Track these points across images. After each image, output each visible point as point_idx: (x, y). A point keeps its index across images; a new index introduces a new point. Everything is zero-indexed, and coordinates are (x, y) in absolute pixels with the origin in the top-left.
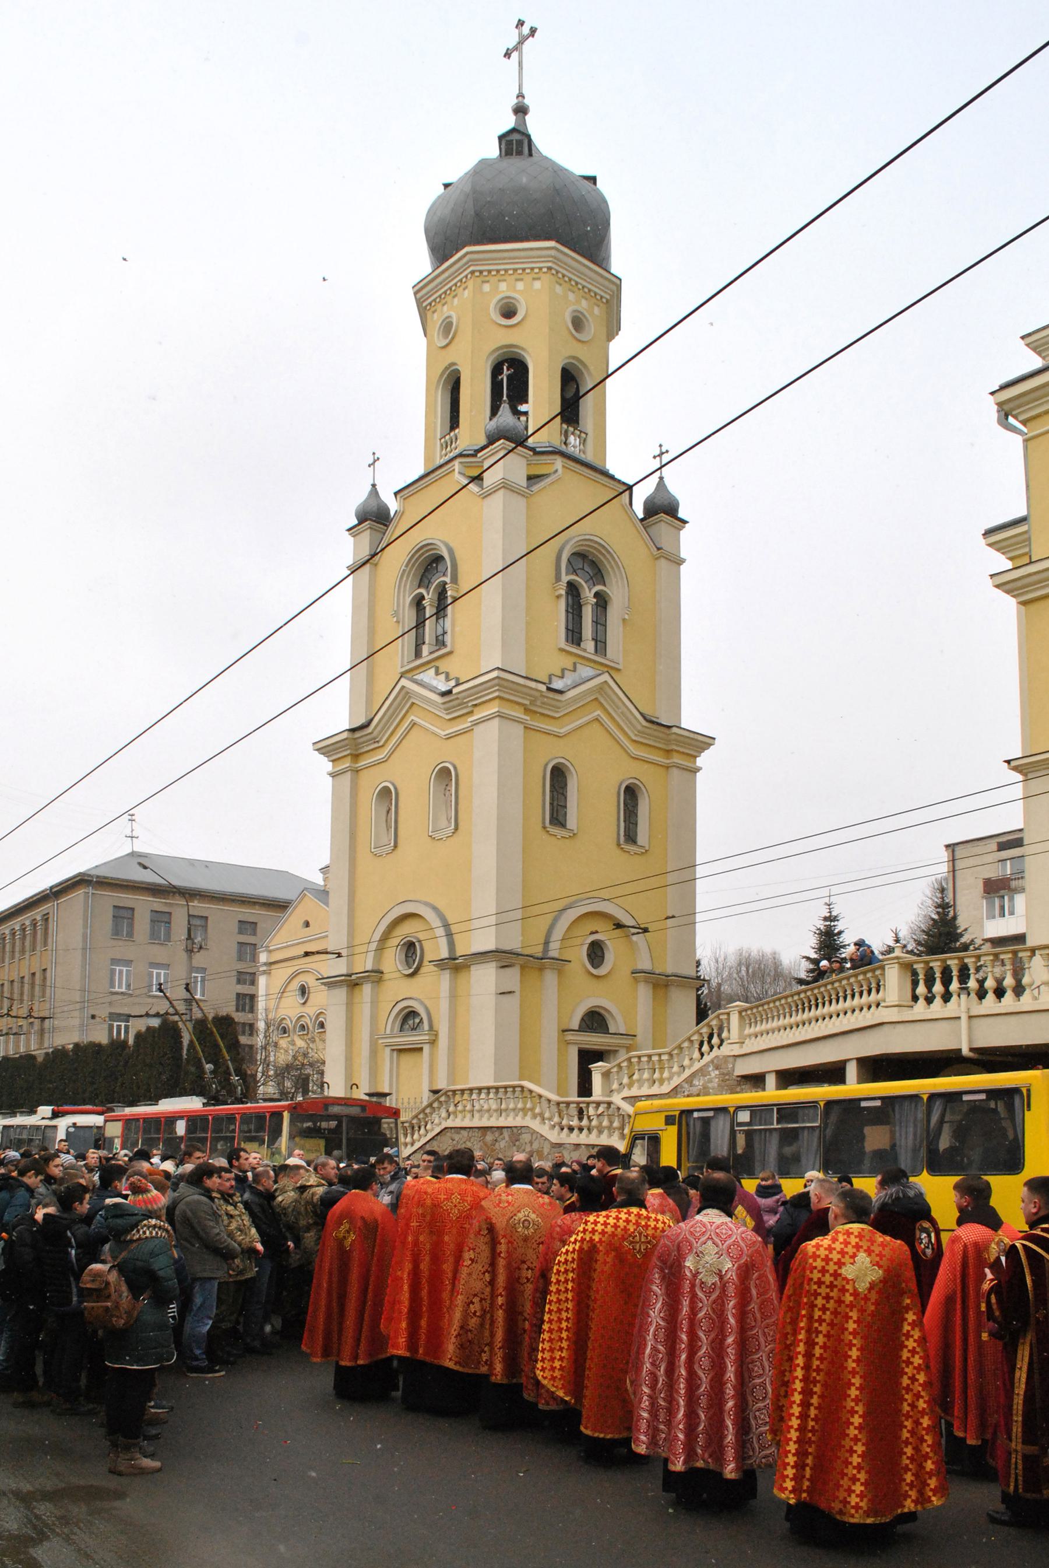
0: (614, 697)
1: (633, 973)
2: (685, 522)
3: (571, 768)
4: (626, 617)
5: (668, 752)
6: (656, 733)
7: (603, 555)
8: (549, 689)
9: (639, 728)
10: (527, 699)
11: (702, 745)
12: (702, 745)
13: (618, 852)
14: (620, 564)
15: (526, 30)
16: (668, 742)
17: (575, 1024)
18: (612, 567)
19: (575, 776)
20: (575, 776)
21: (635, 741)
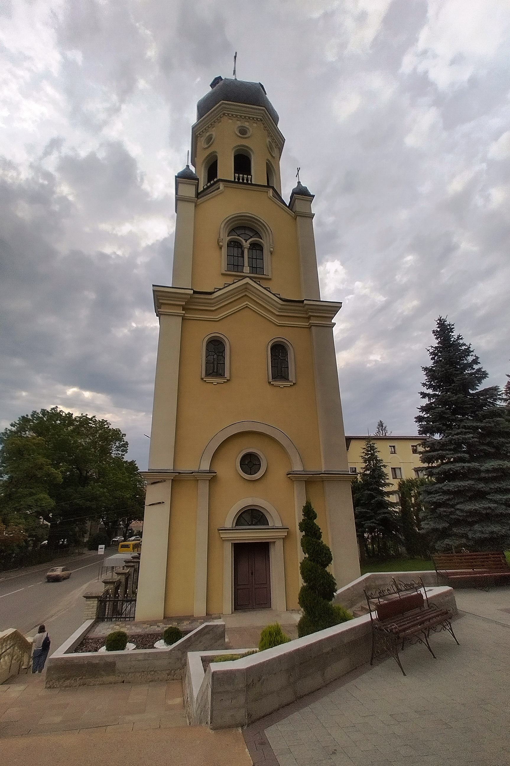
0: (258, 292)
1: (288, 475)
2: (313, 196)
3: (289, 344)
4: (272, 249)
5: (309, 318)
6: (290, 307)
7: (256, 223)
8: (195, 292)
9: (280, 306)
10: (183, 301)
11: (335, 309)
12: (335, 309)
13: (268, 386)
14: (268, 228)
15: (298, 169)
16: (306, 312)
17: (229, 523)
18: (256, 223)
19: (291, 349)
20: (291, 349)
21: (278, 315)
